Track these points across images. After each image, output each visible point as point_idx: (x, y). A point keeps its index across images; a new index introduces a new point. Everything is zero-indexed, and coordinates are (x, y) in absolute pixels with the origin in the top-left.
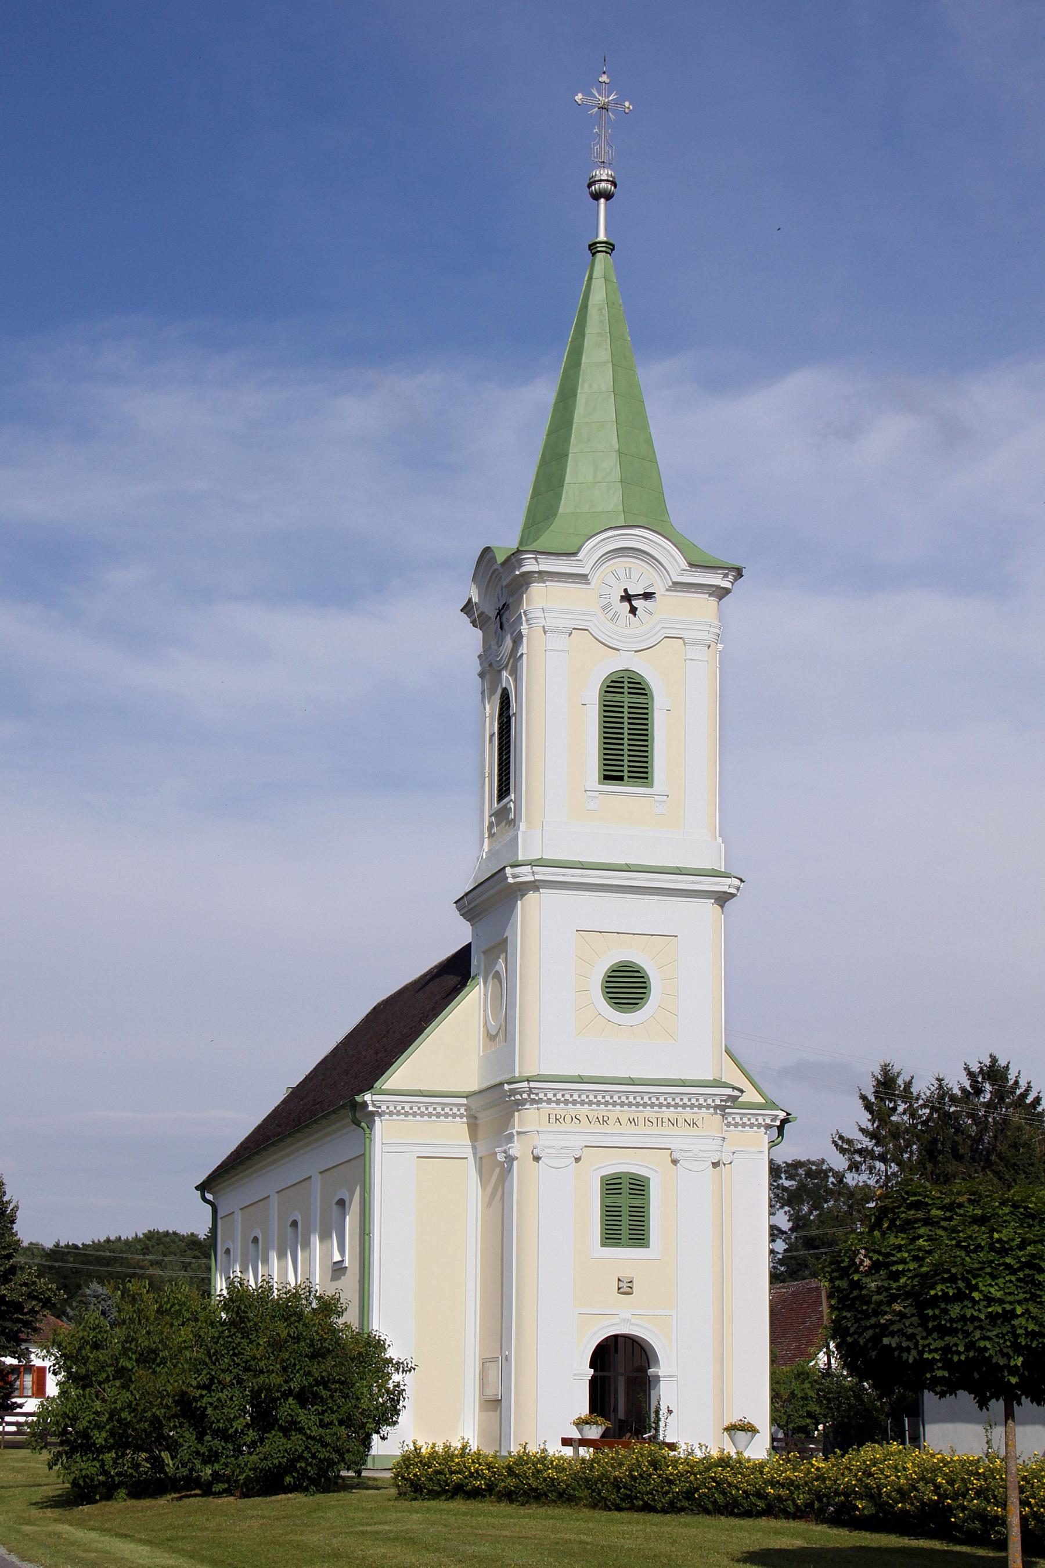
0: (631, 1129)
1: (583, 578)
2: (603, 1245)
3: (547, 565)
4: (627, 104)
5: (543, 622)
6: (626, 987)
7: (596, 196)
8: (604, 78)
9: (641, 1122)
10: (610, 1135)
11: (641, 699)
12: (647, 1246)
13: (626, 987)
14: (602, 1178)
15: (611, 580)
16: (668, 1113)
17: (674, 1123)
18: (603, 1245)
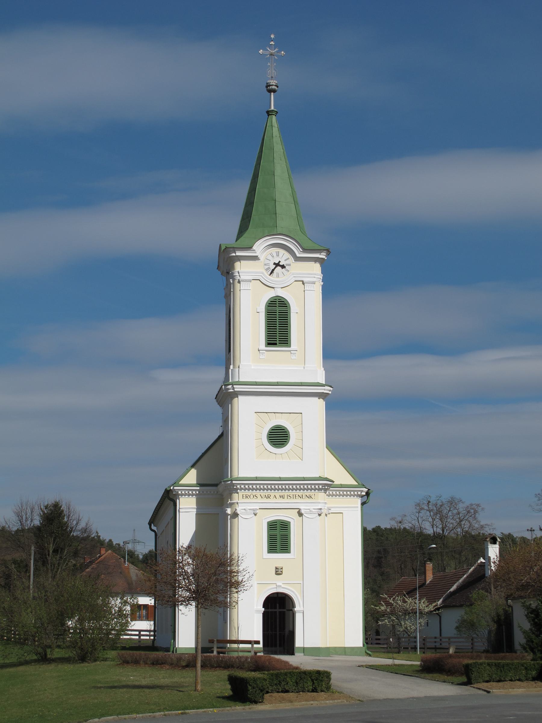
0: (281, 500)
1: (256, 258)
2: (268, 553)
3: (239, 253)
4: (283, 52)
5: (239, 278)
6: (278, 437)
7: (270, 91)
8: (272, 43)
9: (286, 497)
10: (272, 502)
11: (284, 308)
12: (289, 552)
13: (278, 437)
14: (268, 523)
15: (270, 257)
16: (300, 493)
17: (301, 497)
18: (268, 553)
